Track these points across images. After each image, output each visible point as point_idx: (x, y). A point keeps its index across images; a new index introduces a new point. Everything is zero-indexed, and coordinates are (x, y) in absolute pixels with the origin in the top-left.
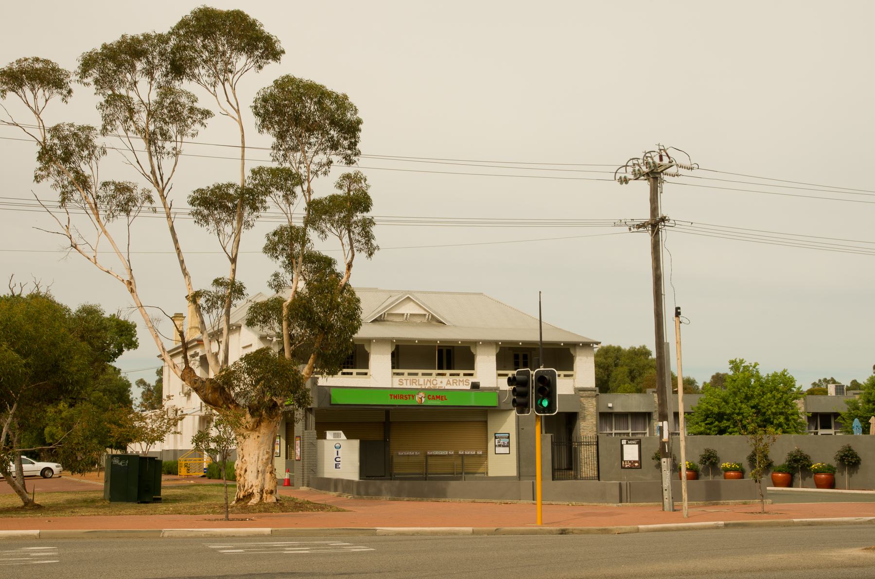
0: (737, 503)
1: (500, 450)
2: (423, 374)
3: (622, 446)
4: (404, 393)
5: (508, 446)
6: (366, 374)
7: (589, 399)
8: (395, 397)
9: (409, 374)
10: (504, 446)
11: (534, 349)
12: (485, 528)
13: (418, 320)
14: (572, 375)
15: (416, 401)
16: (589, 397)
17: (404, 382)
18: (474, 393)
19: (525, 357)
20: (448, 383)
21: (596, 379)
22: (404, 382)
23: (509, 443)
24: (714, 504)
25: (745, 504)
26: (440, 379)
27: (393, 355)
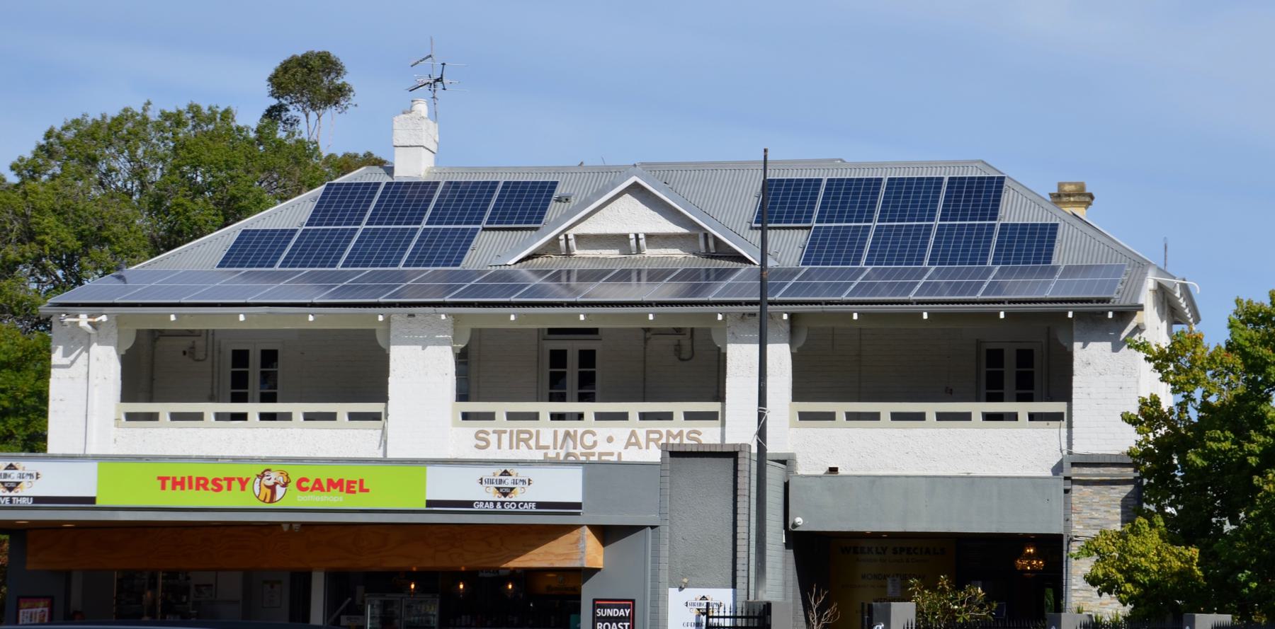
4: (210, 472)
8: (178, 484)
9: (512, 416)
14: (376, 417)
17: (493, 438)
20: (632, 442)
21: (875, 481)
22: (493, 438)
27: (462, 358)
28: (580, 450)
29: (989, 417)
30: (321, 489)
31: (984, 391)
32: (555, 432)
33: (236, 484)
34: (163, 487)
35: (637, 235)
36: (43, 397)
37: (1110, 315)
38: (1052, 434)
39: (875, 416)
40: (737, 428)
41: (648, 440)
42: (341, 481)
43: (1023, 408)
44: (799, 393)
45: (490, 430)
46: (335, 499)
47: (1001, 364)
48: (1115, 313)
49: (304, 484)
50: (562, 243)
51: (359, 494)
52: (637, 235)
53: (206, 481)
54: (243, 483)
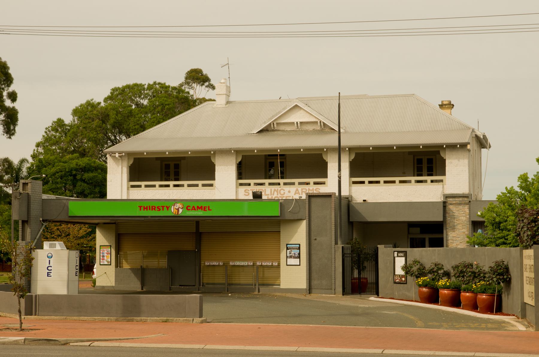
0: (157, 321)
1: (291, 261)
2: (270, 184)
3: (394, 258)
4: (156, 204)
5: (299, 257)
6: (211, 185)
7: (461, 207)
8: (146, 208)
10: (295, 258)
11: (184, 158)
12: (85, 338)
13: (310, 128)
14: (442, 181)
15: (173, 211)
16: (460, 204)
18: (257, 202)
19: (177, 166)
20: (297, 192)
23: (299, 254)
24: (129, 321)
25: (166, 321)
26: (287, 188)
27: (240, 166)
28: (279, 195)
29: (385, 182)
30: (195, 209)
31: (416, 174)
32: (271, 190)
33: (165, 208)
34: (140, 210)
35: (297, 123)
36: (105, 180)
37: (458, 146)
38: (437, 187)
39: (394, 182)
40: (330, 186)
41: (302, 192)
42: (202, 207)
43: (281, 181)
44: (352, 175)
45: (249, 189)
46: (200, 213)
47: (169, 168)
48: (460, 145)
49: (189, 208)
50: (272, 126)
51: (208, 211)
52: (297, 123)
53: (155, 207)
54: (168, 208)
